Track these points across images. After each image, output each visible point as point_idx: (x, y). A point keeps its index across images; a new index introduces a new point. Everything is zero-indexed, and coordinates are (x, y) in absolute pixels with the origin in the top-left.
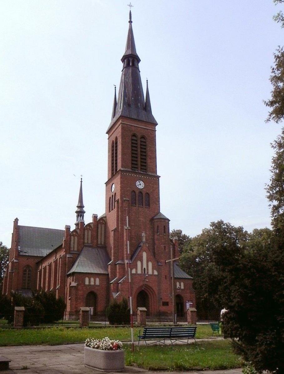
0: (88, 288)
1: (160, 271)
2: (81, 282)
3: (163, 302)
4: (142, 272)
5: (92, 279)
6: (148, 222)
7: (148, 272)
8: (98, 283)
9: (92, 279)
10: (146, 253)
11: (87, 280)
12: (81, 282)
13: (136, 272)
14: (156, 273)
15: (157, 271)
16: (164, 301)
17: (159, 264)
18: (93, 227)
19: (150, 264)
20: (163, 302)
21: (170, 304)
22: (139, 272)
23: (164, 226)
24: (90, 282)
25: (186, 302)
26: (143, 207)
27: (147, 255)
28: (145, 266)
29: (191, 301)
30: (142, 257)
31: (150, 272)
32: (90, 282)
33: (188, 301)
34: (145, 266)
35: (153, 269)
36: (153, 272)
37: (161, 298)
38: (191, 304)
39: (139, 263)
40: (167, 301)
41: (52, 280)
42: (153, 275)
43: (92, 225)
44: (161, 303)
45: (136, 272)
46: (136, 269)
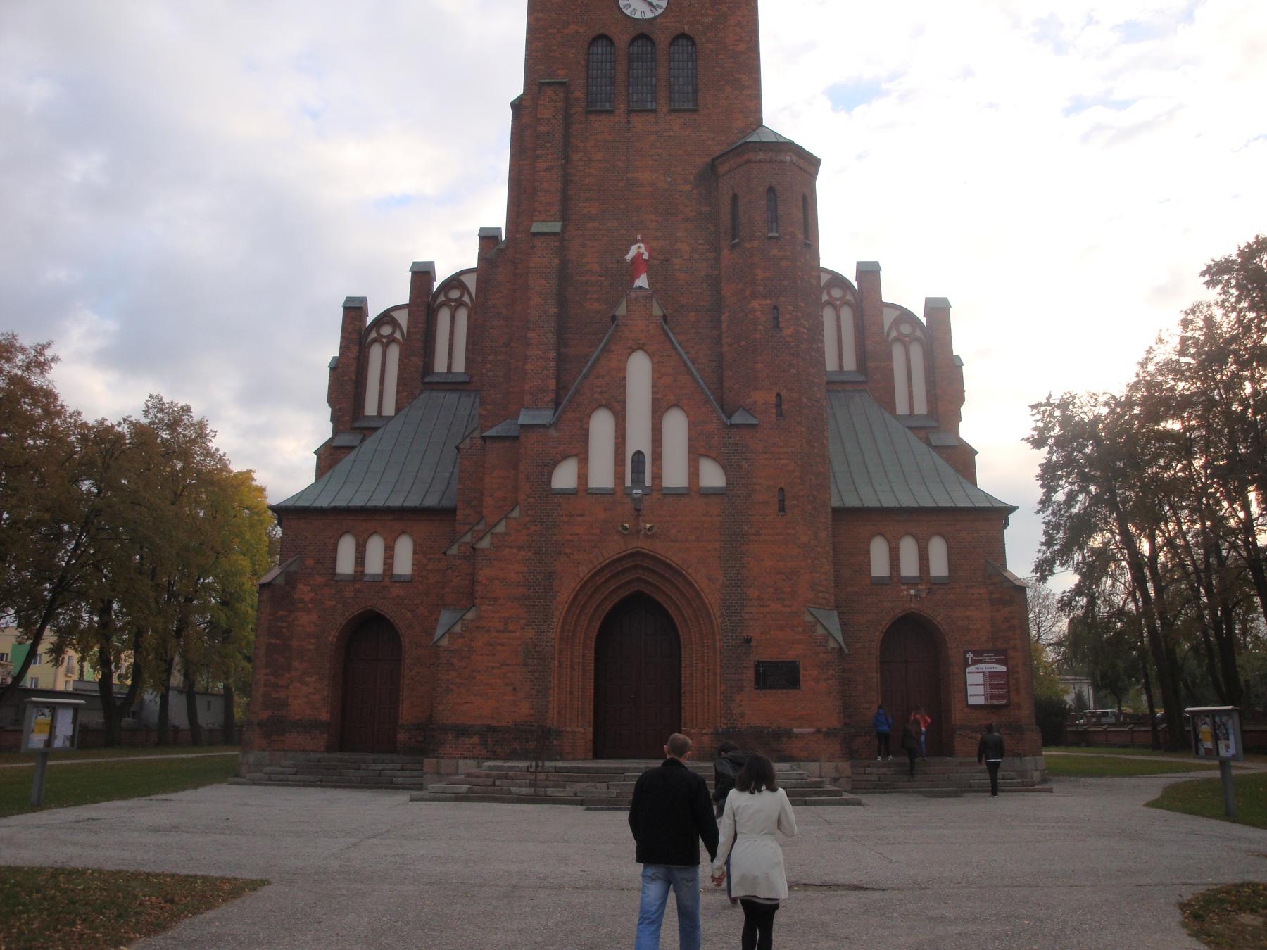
0: (349, 591)
1: (744, 465)
2: (310, 562)
3: (758, 665)
4: (619, 476)
5: (908, 548)
6: (688, 188)
7: (657, 477)
8: (404, 563)
9: (908, 548)
10: (651, 356)
11: (346, 551)
12: (310, 562)
13: (583, 476)
14: (712, 476)
15: (724, 468)
16: (767, 655)
17: (738, 419)
18: (473, 292)
19: (676, 426)
20: (758, 665)
21: (806, 675)
22: (602, 475)
23: (771, 190)
24: (924, 559)
25: (1235, 623)
26: (654, 111)
27: (654, 370)
28: (638, 439)
29: (997, 652)
30: (621, 384)
31: (675, 475)
32: (924, 559)
33: (975, 653)
34: (638, 439)
35: (696, 453)
36: (694, 473)
37: (748, 640)
38: (993, 675)
39: (601, 426)
40: (791, 655)
41: (665, 559)
42: (694, 490)
43: (471, 282)
44: (750, 674)
45: (583, 476)
46: (584, 461)
